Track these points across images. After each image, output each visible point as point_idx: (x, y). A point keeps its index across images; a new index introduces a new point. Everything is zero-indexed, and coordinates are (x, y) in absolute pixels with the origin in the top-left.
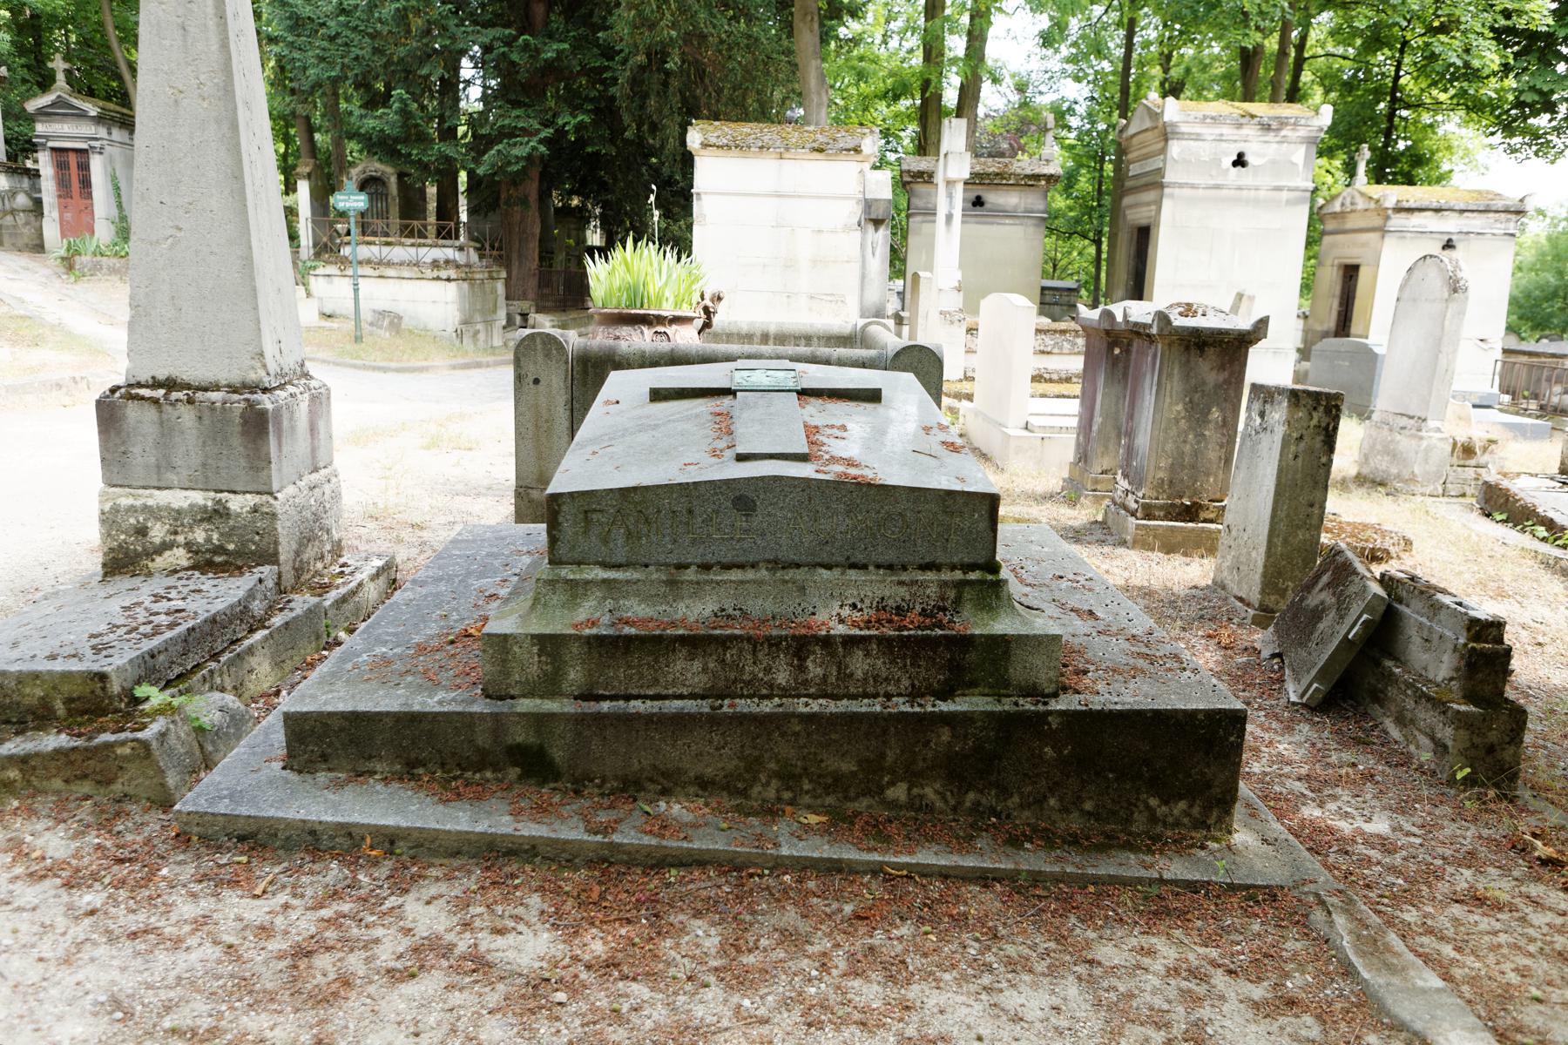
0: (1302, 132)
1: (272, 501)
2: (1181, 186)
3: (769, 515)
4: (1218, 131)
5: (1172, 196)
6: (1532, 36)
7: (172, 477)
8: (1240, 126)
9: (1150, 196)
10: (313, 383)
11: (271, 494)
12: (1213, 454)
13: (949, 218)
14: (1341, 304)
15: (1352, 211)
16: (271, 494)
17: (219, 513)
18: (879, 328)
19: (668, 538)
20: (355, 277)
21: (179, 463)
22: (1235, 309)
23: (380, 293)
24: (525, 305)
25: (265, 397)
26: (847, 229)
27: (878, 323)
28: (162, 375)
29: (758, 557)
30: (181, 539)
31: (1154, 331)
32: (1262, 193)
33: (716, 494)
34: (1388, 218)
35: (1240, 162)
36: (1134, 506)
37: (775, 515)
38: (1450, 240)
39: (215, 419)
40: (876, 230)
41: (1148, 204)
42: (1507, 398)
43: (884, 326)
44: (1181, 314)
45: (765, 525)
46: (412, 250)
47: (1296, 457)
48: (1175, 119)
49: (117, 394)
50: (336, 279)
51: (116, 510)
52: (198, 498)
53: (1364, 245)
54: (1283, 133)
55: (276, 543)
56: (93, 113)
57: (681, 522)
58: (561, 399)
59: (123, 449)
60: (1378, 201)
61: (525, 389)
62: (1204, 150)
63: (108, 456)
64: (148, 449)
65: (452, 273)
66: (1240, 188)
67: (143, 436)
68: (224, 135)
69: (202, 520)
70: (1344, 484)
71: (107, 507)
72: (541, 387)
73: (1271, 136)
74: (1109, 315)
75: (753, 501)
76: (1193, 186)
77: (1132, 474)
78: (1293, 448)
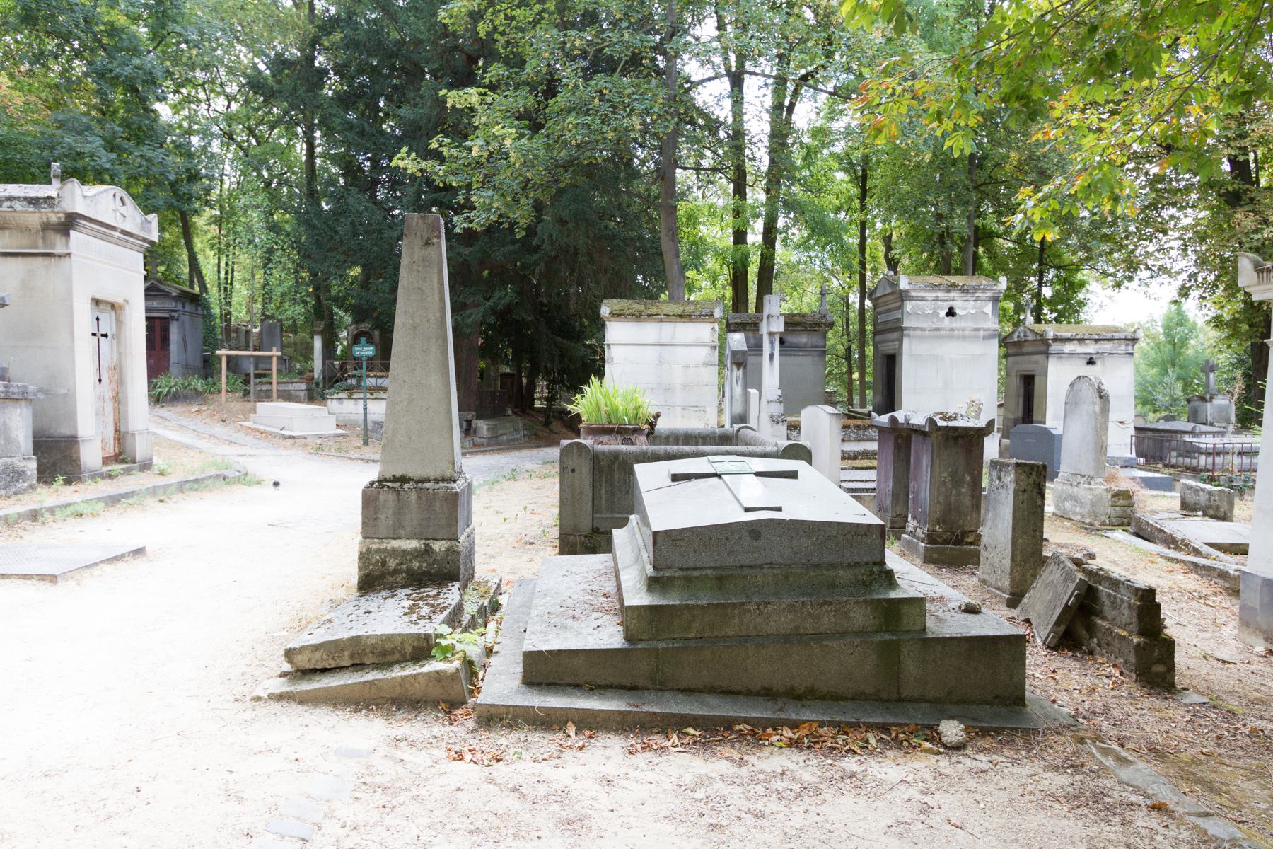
0: (989, 294)
2: (914, 329)
4: (935, 295)
7: (402, 532)
8: (949, 291)
9: (895, 335)
12: (967, 501)
13: (772, 356)
14: (1024, 401)
15: (1026, 341)
17: (428, 551)
20: (365, 399)
22: (977, 416)
24: (470, 415)
26: (706, 364)
28: (398, 474)
29: (762, 562)
30: (404, 567)
32: (967, 332)
34: (1049, 345)
35: (951, 313)
36: (923, 536)
38: (1091, 358)
39: (428, 500)
41: (893, 341)
42: (1142, 460)
44: (941, 418)
50: (345, 401)
51: (369, 550)
52: (413, 544)
53: (1036, 362)
55: (459, 568)
56: (174, 294)
58: (587, 482)
60: (1042, 335)
61: (566, 476)
62: (928, 307)
66: (952, 330)
70: (623, 569)
71: (364, 550)
73: (969, 297)
74: (894, 420)
76: (922, 329)
78: (1021, 497)
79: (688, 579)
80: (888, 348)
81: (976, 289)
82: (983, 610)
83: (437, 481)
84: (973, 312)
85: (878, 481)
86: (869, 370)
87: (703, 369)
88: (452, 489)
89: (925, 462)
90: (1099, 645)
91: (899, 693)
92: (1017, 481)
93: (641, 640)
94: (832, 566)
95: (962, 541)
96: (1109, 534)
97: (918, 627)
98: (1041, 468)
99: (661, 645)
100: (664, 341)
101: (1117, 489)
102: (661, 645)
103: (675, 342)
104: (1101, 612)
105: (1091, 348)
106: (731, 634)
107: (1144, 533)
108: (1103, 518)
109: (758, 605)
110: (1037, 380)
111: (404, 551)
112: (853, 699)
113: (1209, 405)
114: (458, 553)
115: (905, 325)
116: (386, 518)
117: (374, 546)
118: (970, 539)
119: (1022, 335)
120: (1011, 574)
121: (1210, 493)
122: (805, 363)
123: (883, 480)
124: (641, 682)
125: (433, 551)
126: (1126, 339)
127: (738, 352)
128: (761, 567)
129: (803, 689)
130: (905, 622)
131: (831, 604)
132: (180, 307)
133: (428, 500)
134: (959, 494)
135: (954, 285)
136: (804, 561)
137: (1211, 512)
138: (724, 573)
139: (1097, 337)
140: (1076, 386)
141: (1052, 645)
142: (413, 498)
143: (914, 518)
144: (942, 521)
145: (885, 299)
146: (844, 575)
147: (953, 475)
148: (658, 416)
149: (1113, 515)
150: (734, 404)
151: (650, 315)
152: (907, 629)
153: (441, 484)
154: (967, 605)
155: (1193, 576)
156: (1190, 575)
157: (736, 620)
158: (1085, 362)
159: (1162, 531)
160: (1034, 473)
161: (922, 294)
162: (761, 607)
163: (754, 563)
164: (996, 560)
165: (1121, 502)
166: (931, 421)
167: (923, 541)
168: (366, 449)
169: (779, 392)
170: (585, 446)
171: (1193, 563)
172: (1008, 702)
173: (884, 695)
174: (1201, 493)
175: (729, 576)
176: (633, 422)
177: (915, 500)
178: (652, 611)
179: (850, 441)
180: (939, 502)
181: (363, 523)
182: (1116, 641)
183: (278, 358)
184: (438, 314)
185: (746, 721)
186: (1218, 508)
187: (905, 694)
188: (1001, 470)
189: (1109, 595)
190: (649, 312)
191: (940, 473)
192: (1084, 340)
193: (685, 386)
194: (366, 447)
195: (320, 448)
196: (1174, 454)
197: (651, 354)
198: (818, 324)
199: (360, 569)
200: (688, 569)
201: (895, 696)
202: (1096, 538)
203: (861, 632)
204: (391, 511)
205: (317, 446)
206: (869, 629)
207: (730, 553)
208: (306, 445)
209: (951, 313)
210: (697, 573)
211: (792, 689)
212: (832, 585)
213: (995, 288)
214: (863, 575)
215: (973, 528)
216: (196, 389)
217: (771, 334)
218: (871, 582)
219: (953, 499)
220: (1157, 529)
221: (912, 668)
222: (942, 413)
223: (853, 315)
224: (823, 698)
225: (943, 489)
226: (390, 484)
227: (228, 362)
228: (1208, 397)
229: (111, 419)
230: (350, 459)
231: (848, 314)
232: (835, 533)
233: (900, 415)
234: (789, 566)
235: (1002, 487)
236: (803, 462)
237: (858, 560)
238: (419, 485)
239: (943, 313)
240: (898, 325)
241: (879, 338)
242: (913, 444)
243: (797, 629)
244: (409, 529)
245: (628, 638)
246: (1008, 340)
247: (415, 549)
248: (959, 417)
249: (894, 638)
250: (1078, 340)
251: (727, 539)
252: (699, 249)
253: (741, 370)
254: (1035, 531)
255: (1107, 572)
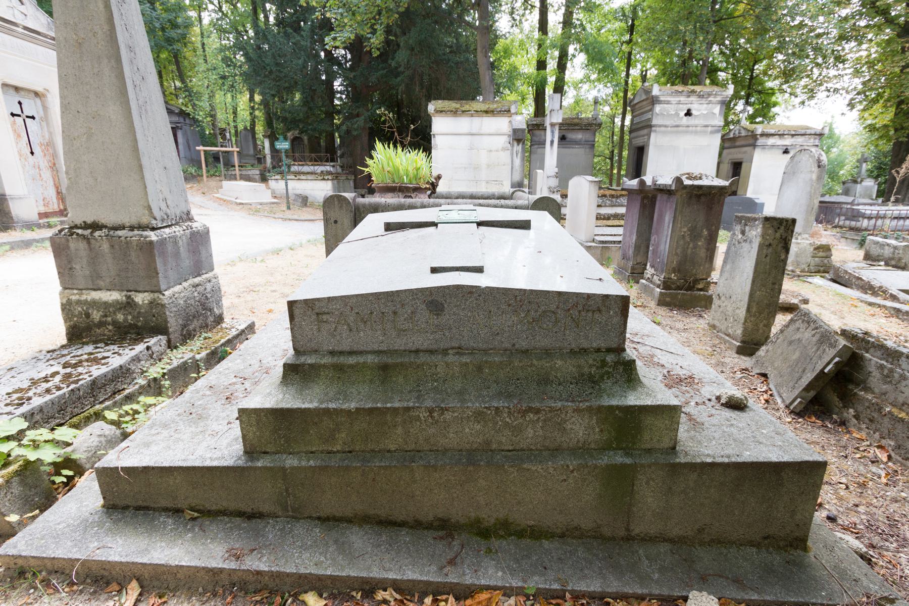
0: (719, 98)
1: (161, 296)
2: (660, 126)
3: (454, 314)
4: (678, 99)
5: (655, 131)
6: (640, 154)
8: (689, 96)
9: (645, 131)
10: (194, 225)
11: (160, 292)
12: (702, 253)
13: (552, 142)
15: (739, 137)
16: (160, 292)
17: (129, 304)
18: (521, 193)
19: (379, 332)
21: (104, 274)
23: (298, 186)
25: (152, 233)
26: (504, 149)
27: (519, 191)
28: (89, 220)
29: (447, 346)
30: (109, 319)
31: (673, 188)
32: (699, 129)
33: (414, 299)
34: (756, 139)
35: (688, 113)
36: (659, 282)
37: (459, 314)
38: (787, 149)
39: (122, 249)
40: (518, 145)
41: (643, 136)
43: (523, 191)
44: (687, 178)
45: (451, 322)
46: (312, 167)
47: (766, 256)
48: (658, 93)
49: (63, 233)
50: (280, 181)
52: (114, 296)
53: (745, 152)
54: (710, 99)
56: (177, 111)
57: (388, 320)
59: (69, 266)
60: (753, 132)
61: (330, 226)
62: (671, 109)
63: (62, 271)
64: (84, 266)
65: (330, 177)
66: (688, 126)
67: (81, 258)
68: (113, 67)
69: (120, 309)
71: (64, 301)
72: (339, 225)
73: (704, 101)
74: (642, 183)
75: (441, 304)
76: (666, 126)
77: (656, 266)
78: (765, 251)
79: (339, 368)
80: (639, 142)
81: (709, 95)
82: (751, 402)
83: (132, 228)
84: (705, 112)
85: (624, 235)
86: (624, 167)
87: (502, 153)
88: (146, 237)
89: (668, 218)
90: (857, 417)
91: (628, 530)
92: (763, 236)
93: (265, 453)
94: (547, 353)
95: (694, 287)
96: (810, 279)
97: (666, 443)
98: (790, 222)
99: (291, 462)
100: (474, 131)
101: (819, 243)
102: (291, 462)
103: (482, 132)
104: (864, 382)
105: (787, 141)
106: (392, 447)
107: (840, 279)
108: (803, 266)
109: (431, 411)
110: (744, 165)
111: (105, 303)
112: (562, 536)
113: (859, 186)
114: (163, 306)
115: (654, 122)
116: (81, 268)
117: (74, 298)
118: (700, 286)
119: (737, 132)
120: (744, 324)
121: (895, 248)
122: (578, 154)
123: (628, 234)
124: (266, 508)
125: (136, 304)
126: (815, 134)
127: (519, 130)
128: (445, 352)
129: (493, 521)
130: (646, 436)
131: (537, 411)
132: (182, 120)
133: (122, 249)
134: (695, 248)
135: (693, 92)
136: (507, 345)
137: (893, 263)
138: (390, 361)
139: (793, 133)
140: (796, 159)
141: (798, 411)
142: (106, 246)
143: (652, 266)
144: (677, 270)
145: (640, 105)
146: (564, 367)
147: (693, 230)
148: (439, 177)
149: (813, 263)
150: (514, 173)
151: (463, 111)
152: (648, 446)
153: (136, 232)
154: (731, 398)
155: (894, 320)
156: (891, 319)
157: (400, 430)
158: (782, 151)
159: (861, 279)
160: (782, 228)
161: (669, 99)
162: (435, 414)
163: (435, 347)
164: (730, 309)
165: (821, 254)
166: (678, 180)
167: (658, 286)
168: (288, 212)
169: (556, 170)
170: (345, 199)
171: (895, 308)
172: (782, 544)
173: (607, 531)
174: (887, 247)
175: (396, 365)
176: (414, 182)
177: (655, 252)
178: (279, 415)
179: (605, 206)
180: (676, 254)
181: (59, 273)
182: (886, 420)
183: (238, 152)
184: (106, 27)
185: (397, 586)
186: (900, 259)
187: (637, 530)
188: (746, 225)
189: (882, 367)
190: (463, 109)
191: (681, 228)
192: (783, 135)
193: (488, 166)
194: (289, 211)
195: (257, 211)
196: (843, 218)
197: (465, 140)
198: (590, 125)
199: (66, 322)
200: (341, 353)
201: (622, 533)
202: (798, 283)
203: (580, 450)
204: (85, 261)
205: (253, 209)
206: (593, 446)
207: (401, 332)
208: (250, 209)
209: (688, 113)
210: (352, 360)
211: (478, 521)
212: (544, 380)
213: (724, 93)
214: (591, 366)
215: (704, 277)
216: (191, 174)
217: (552, 125)
218: (602, 377)
219: (689, 251)
220: (855, 277)
221: (650, 500)
222: (688, 174)
223: (617, 130)
224: (520, 534)
225: (681, 242)
226: (80, 231)
227: (205, 154)
228: (859, 180)
229: (51, 183)
230: (275, 218)
231: (613, 129)
232: (553, 307)
233: (648, 179)
234: (485, 351)
235: (745, 241)
236: (546, 212)
237: (585, 344)
238: (112, 233)
239: (682, 114)
240: (649, 123)
241: (633, 135)
242: (657, 203)
243: (488, 443)
244: (108, 280)
245: (250, 452)
246: (725, 137)
247: (117, 301)
248: (704, 177)
249: (628, 461)
250: (779, 135)
251: (395, 313)
252: (513, 74)
253: (520, 145)
254: (774, 284)
255: (878, 339)
